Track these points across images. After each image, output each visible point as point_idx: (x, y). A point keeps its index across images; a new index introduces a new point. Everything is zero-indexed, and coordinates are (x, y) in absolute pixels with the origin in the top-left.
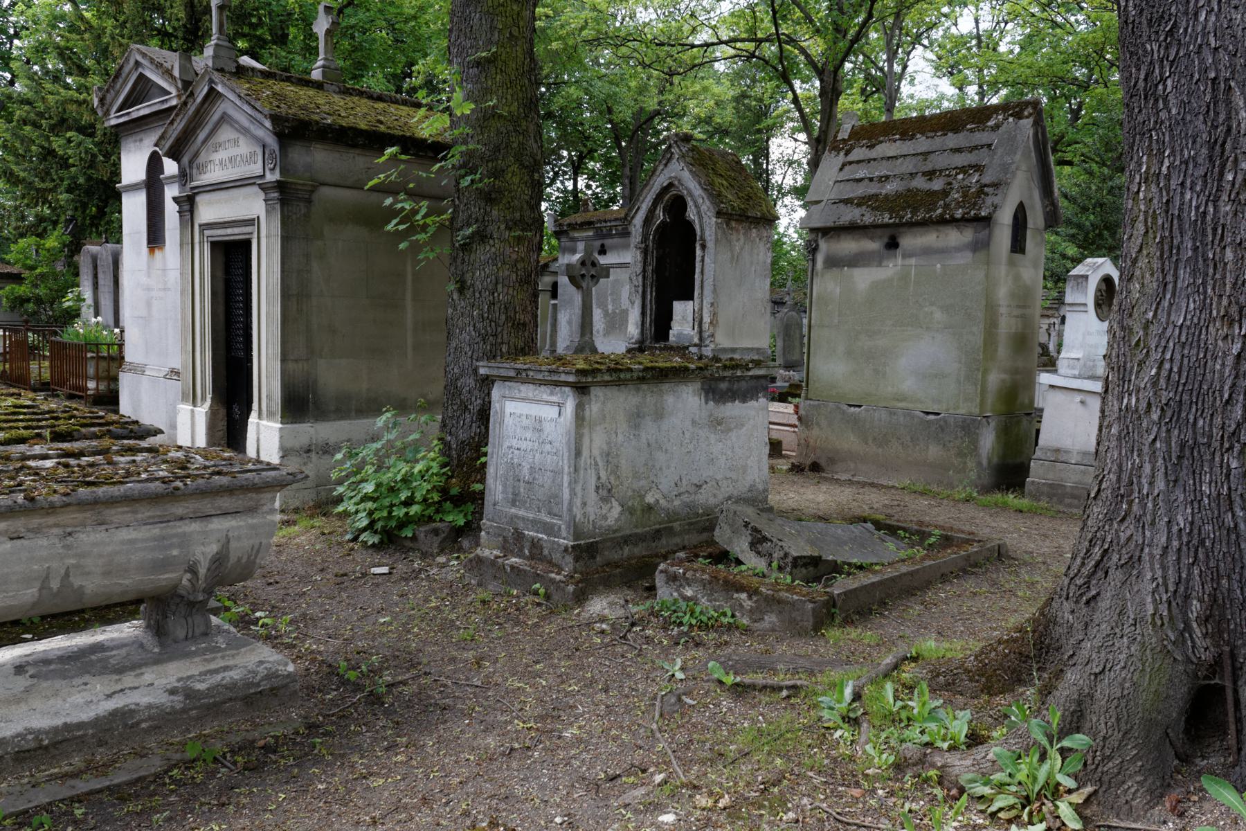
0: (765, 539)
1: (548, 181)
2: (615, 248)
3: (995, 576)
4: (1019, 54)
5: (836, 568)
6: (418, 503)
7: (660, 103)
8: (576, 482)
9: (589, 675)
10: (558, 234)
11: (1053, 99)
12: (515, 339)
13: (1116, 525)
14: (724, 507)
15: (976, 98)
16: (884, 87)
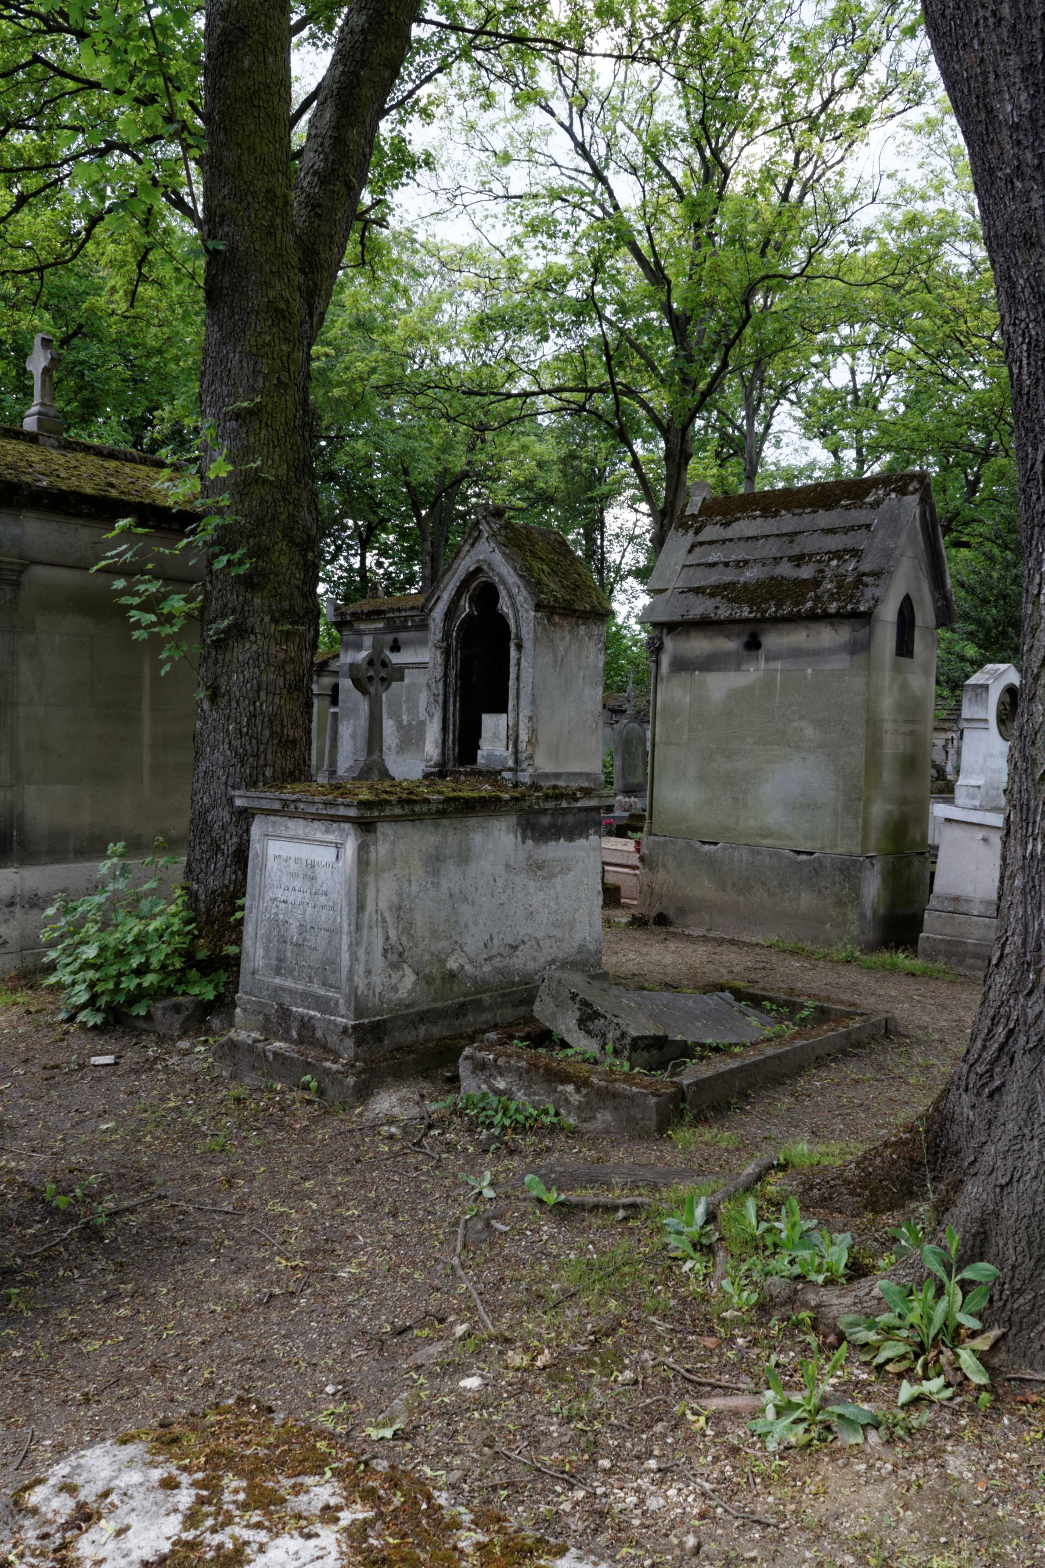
0: (597, 1015)
1: (328, 557)
2: (411, 643)
3: (881, 1059)
4: (905, 413)
5: (686, 1051)
6: (154, 971)
7: (469, 463)
8: (358, 944)
9: (373, 1194)
10: (340, 625)
11: (945, 468)
12: (282, 762)
13: (1022, 1000)
14: (546, 974)
15: (854, 466)
16: (745, 449)
